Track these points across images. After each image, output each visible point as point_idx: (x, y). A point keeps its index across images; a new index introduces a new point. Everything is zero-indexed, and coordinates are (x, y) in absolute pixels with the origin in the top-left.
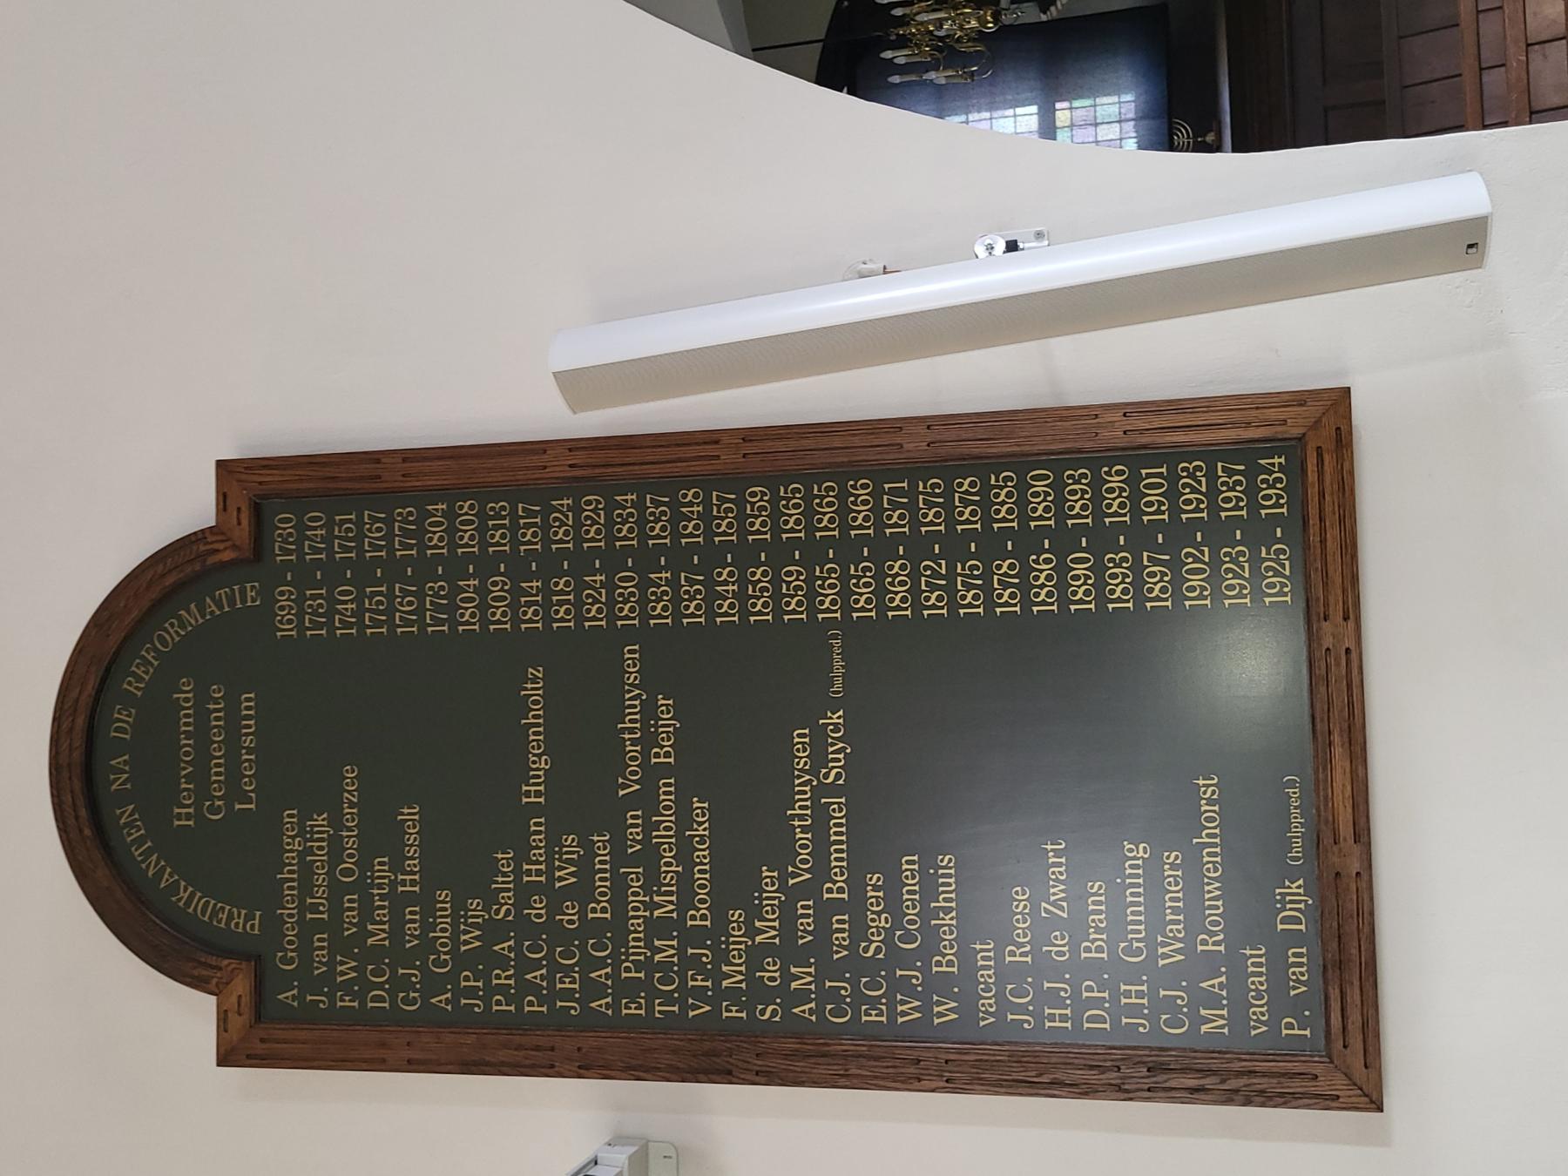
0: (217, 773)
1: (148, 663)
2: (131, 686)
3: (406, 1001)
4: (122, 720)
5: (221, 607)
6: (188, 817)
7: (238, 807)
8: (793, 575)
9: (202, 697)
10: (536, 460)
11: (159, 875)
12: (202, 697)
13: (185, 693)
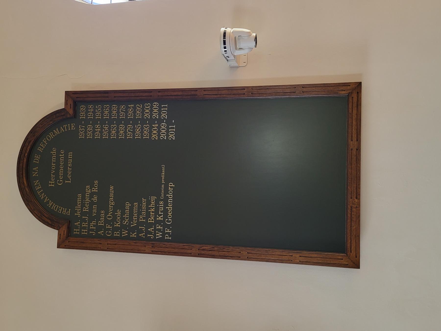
0: (61, 173)
1: (44, 143)
3: (108, 233)
4: (37, 158)
5: (64, 130)
6: (53, 184)
9: (58, 153)
12: (58, 153)
13: (54, 152)
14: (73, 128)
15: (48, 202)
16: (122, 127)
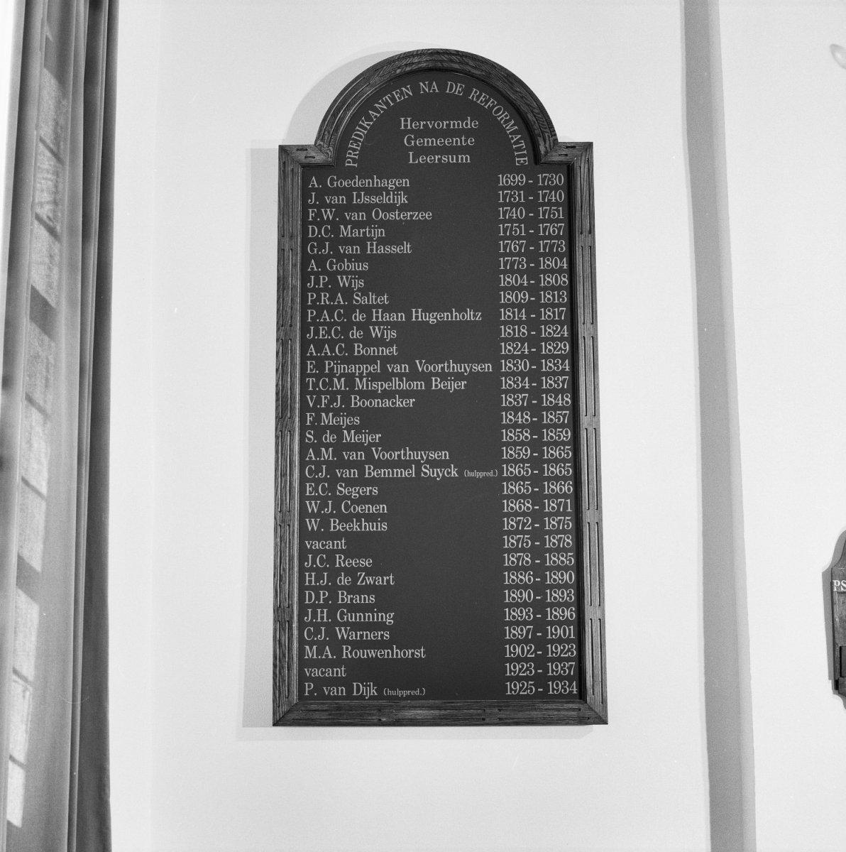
0: (428, 142)
1: (487, 101)
2: (474, 93)
3: (312, 246)
6: (406, 126)
8: (526, 453)
9: (468, 133)
13: (470, 124)
14: (518, 162)
15: (369, 118)
16: (520, 197)
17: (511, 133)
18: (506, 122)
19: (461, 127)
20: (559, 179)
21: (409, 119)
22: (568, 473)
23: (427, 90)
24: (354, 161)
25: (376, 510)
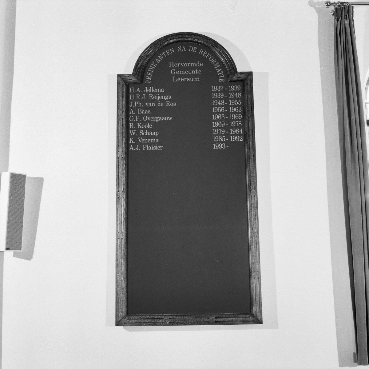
0: (181, 72)
1: (206, 55)
2: (201, 51)
3: (132, 118)
6: (172, 65)
7: (174, 77)
8: (223, 124)
9: (199, 68)
10: (250, 109)
11: (159, 59)
12: (199, 68)
13: (200, 64)
14: (220, 80)
15: (156, 62)
17: (217, 68)
18: (215, 63)
19: (195, 66)
20: (238, 88)
21: (173, 62)
22: (240, 103)
23: (181, 50)
24: (149, 80)
25: (159, 149)
